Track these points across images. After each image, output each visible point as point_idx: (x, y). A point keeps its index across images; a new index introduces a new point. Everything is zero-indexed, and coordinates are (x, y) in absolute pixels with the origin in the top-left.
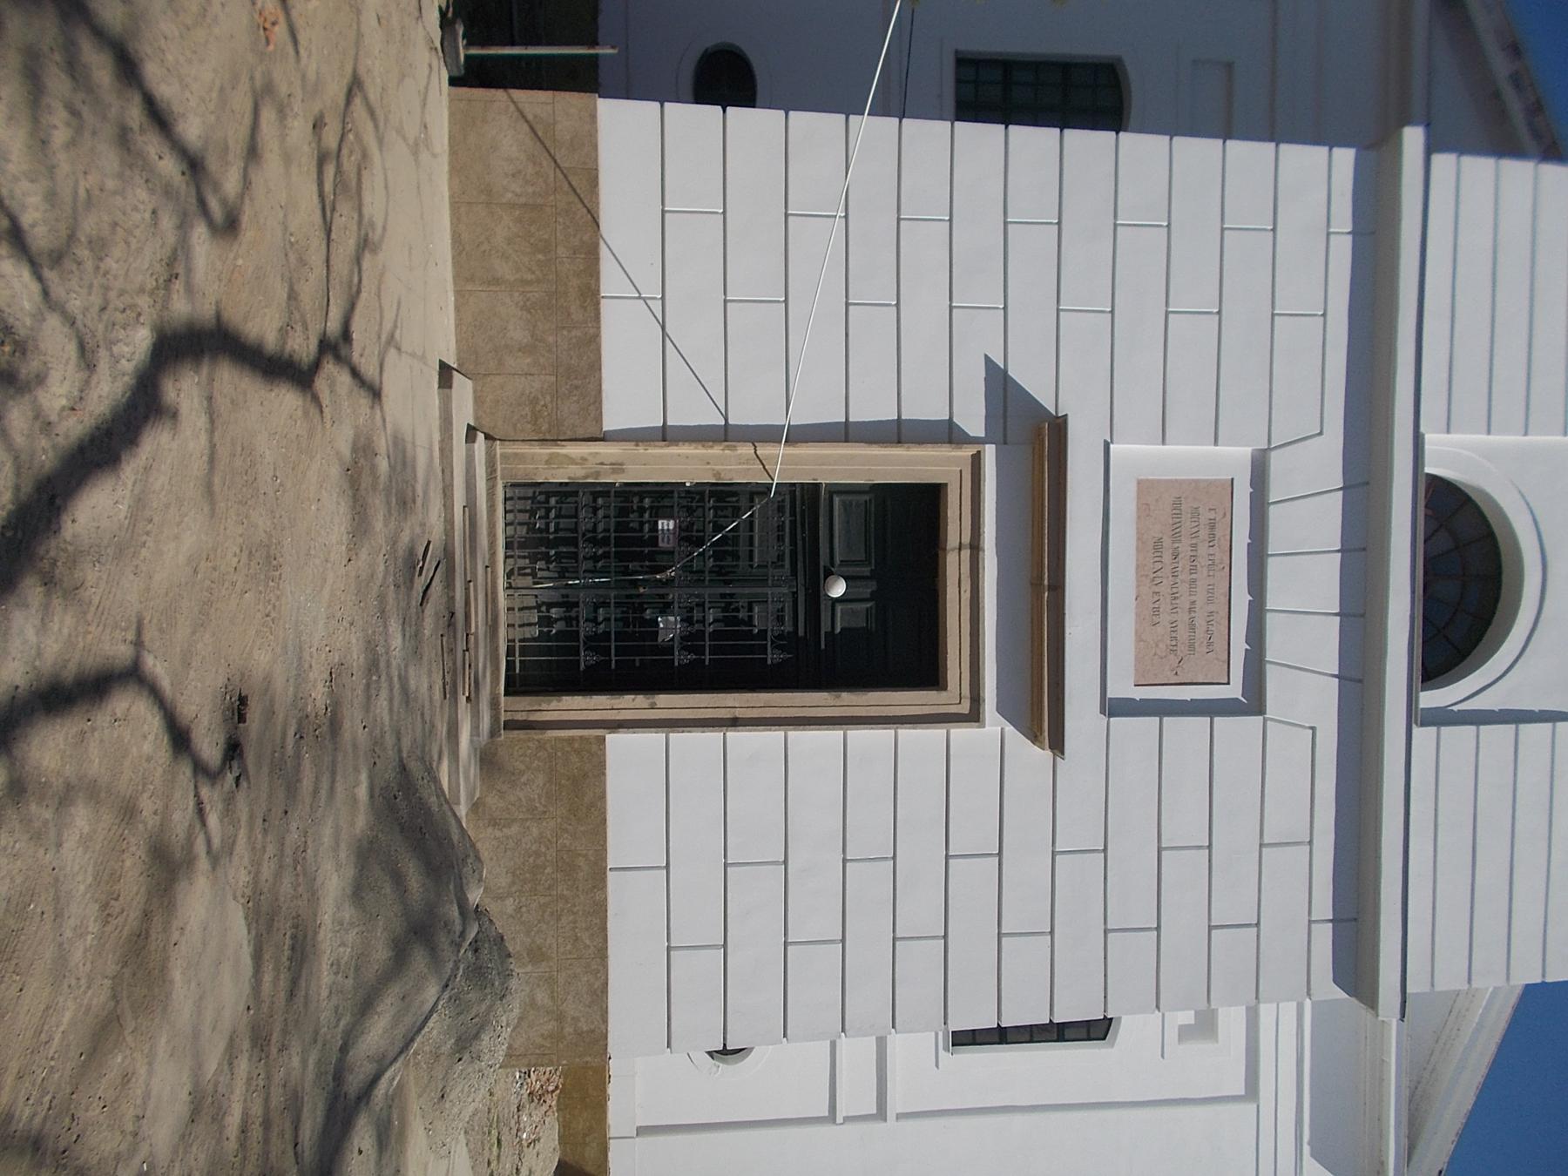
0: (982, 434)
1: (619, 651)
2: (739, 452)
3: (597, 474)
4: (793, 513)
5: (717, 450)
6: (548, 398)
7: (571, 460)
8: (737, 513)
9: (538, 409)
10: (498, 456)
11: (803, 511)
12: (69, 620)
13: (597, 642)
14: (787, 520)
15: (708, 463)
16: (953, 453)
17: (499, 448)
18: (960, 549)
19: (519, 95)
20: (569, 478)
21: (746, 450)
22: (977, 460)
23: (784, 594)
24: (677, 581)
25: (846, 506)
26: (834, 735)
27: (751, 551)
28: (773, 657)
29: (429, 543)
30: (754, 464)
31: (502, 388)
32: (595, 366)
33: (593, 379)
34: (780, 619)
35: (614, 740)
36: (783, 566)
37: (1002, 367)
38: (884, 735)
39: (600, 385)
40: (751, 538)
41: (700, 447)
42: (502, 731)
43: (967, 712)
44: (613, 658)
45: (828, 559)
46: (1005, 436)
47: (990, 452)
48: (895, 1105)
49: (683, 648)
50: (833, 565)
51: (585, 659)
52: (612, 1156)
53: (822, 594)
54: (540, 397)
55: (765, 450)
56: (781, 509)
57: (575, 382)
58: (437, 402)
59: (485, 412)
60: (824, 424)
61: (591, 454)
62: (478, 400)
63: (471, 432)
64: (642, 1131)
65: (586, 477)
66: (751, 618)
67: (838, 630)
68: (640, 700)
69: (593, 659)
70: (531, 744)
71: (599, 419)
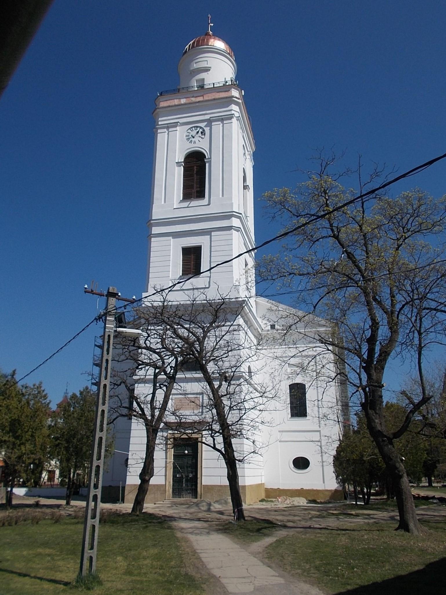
5: (168, 469)
12: (204, 577)
13: (192, 486)
17: (166, 498)
19: (125, 495)
21: (168, 465)
25: (177, 451)
32: (157, 485)
35: (203, 484)
48: (317, 428)
51: (194, 487)
52: (329, 489)
55: (168, 462)
64: (324, 482)
68: (198, 480)
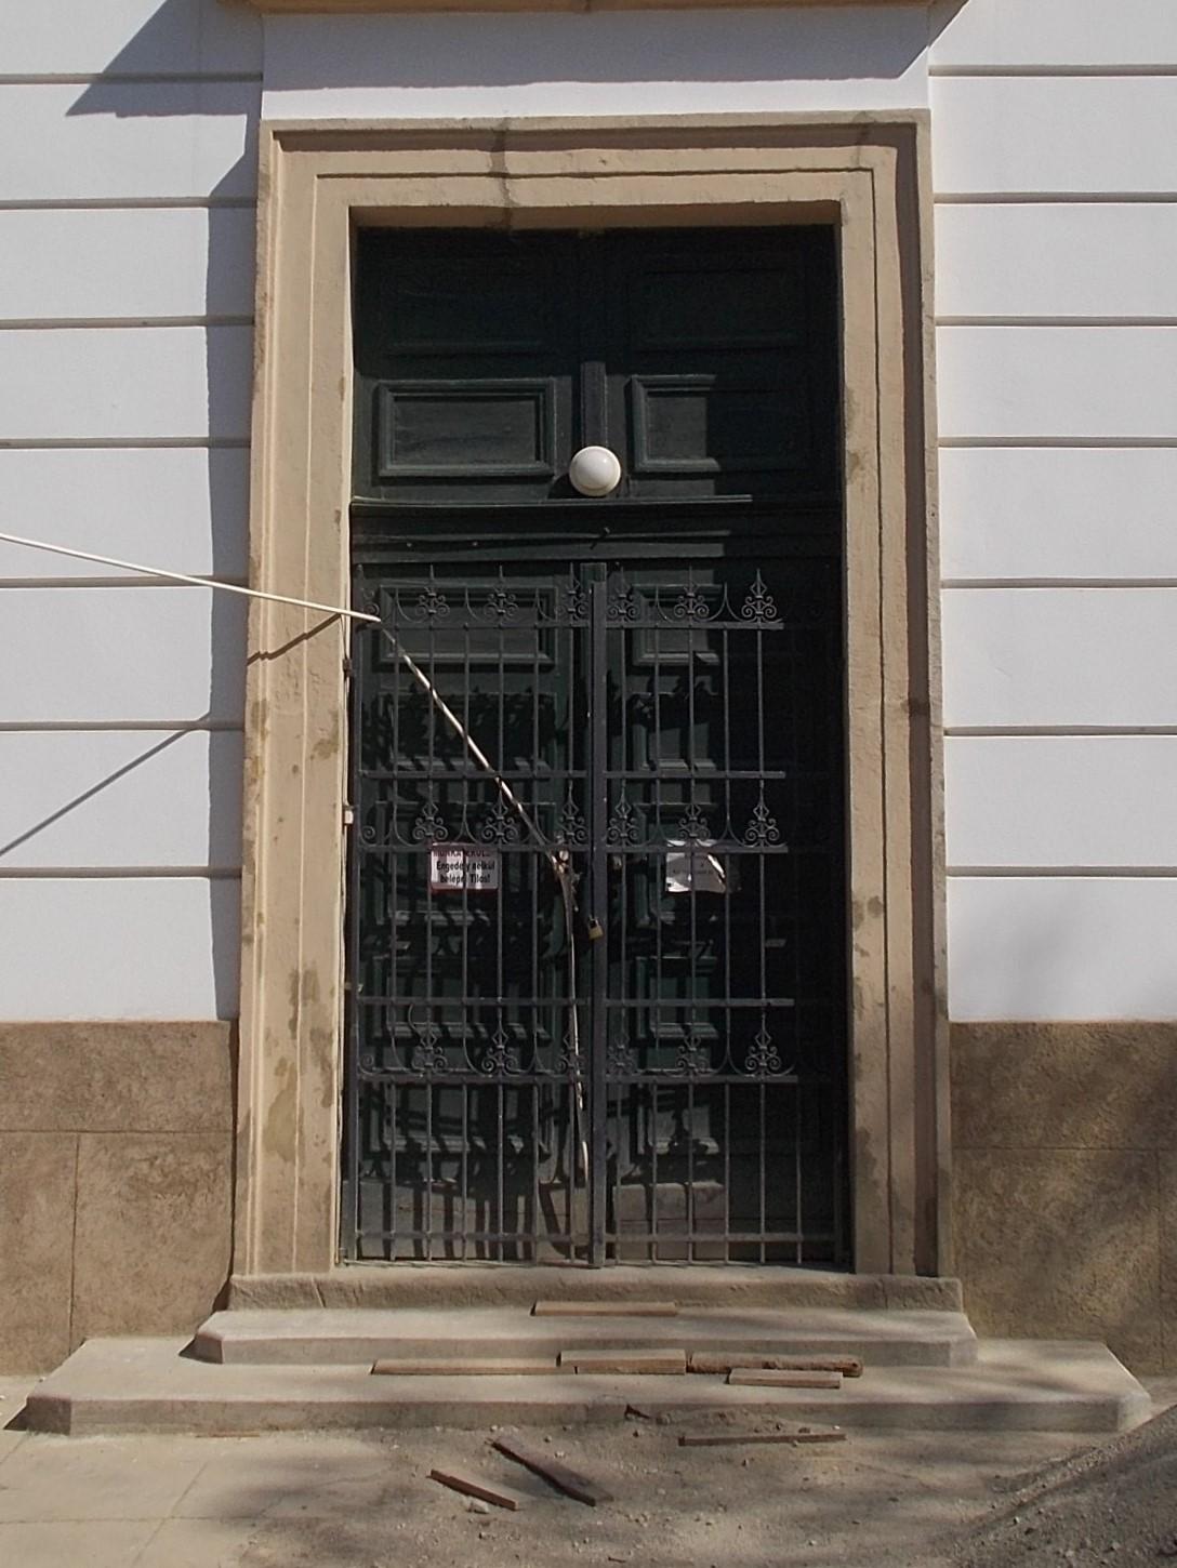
0: (240, 122)
1: (746, 987)
2: (268, 695)
3: (320, 1037)
4: (420, 570)
5: (264, 750)
6: (133, 1152)
7: (283, 1100)
8: (417, 702)
9: (156, 1177)
10: (267, 1277)
11: (418, 546)
14: (433, 584)
15: (296, 769)
16: (280, 196)
17: (250, 1275)
18: (505, 176)
20: (327, 1103)
21: (264, 680)
22: (295, 139)
23: (611, 591)
24: (579, 848)
25: (409, 445)
26: (950, 470)
27: (509, 668)
28: (761, 617)
29: (436, 1476)
30: (299, 663)
31: (106, 1265)
32: (62, 1038)
33: (92, 1044)
34: (669, 600)
36: (547, 596)
37: (86, 86)
38: (947, 352)
39: (106, 1026)
40: (477, 668)
41: (256, 788)
42: (941, 1280)
43: (894, 151)
44: (763, 1001)
45: (531, 489)
46: (242, 78)
47: (284, 107)
49: (740, 832)
50: (545, 478)
51: (764, 1068)
53: (610, 501)
54: (131, 1172)
55: (266, 633)
56: (409, 599)
57: (97, 1087)
58: (101, 1439)
59: (161, 1309)
60: (211, 487)
61: (268, 1053)
62: (133, 1324)
63: (204, 1350)
65: (325, 1064)
66: (667, 670)
67: (711, 463)
68: (865, 937)
69: (764, 1052)
70: (973, 1210)
71: (187, 1031)
